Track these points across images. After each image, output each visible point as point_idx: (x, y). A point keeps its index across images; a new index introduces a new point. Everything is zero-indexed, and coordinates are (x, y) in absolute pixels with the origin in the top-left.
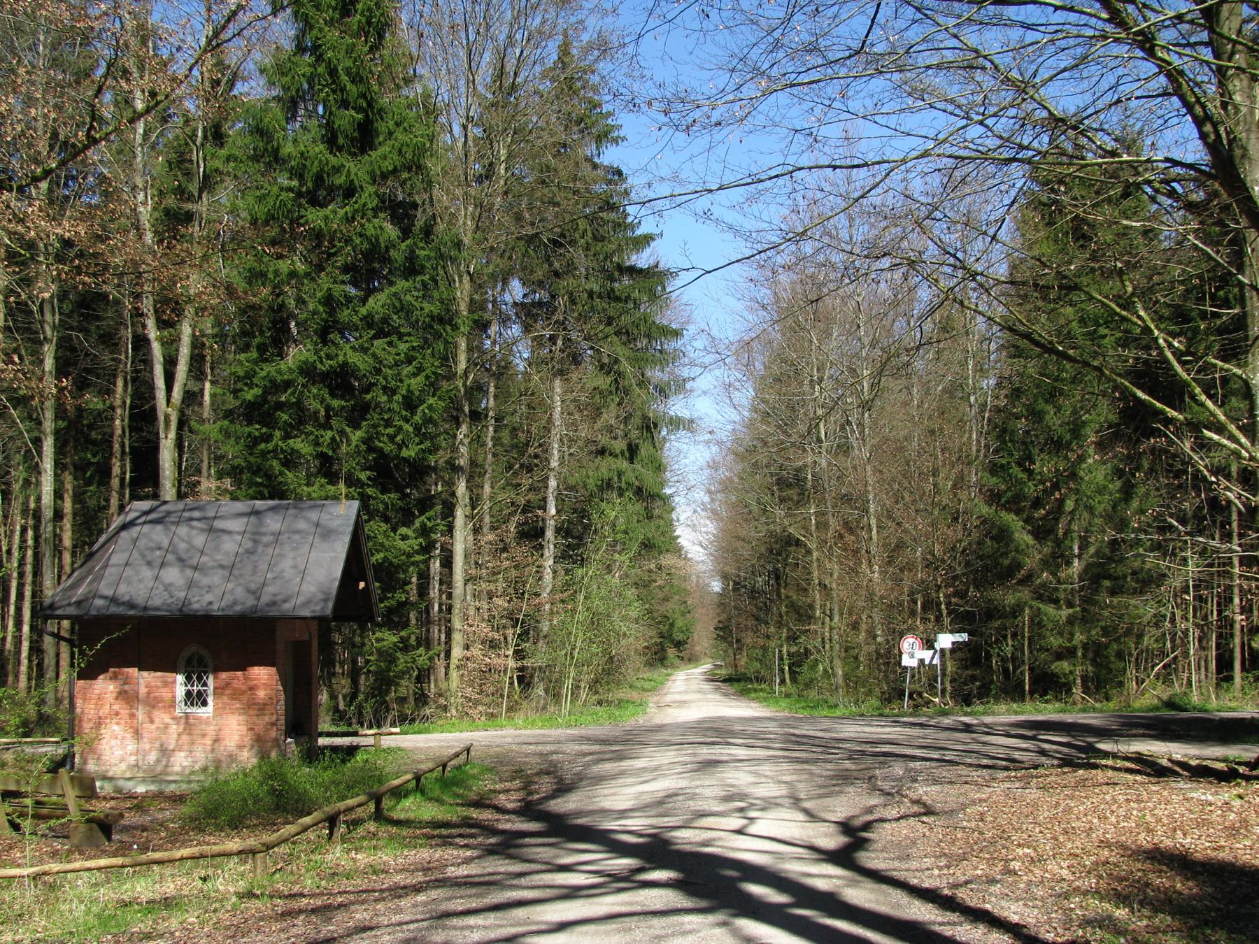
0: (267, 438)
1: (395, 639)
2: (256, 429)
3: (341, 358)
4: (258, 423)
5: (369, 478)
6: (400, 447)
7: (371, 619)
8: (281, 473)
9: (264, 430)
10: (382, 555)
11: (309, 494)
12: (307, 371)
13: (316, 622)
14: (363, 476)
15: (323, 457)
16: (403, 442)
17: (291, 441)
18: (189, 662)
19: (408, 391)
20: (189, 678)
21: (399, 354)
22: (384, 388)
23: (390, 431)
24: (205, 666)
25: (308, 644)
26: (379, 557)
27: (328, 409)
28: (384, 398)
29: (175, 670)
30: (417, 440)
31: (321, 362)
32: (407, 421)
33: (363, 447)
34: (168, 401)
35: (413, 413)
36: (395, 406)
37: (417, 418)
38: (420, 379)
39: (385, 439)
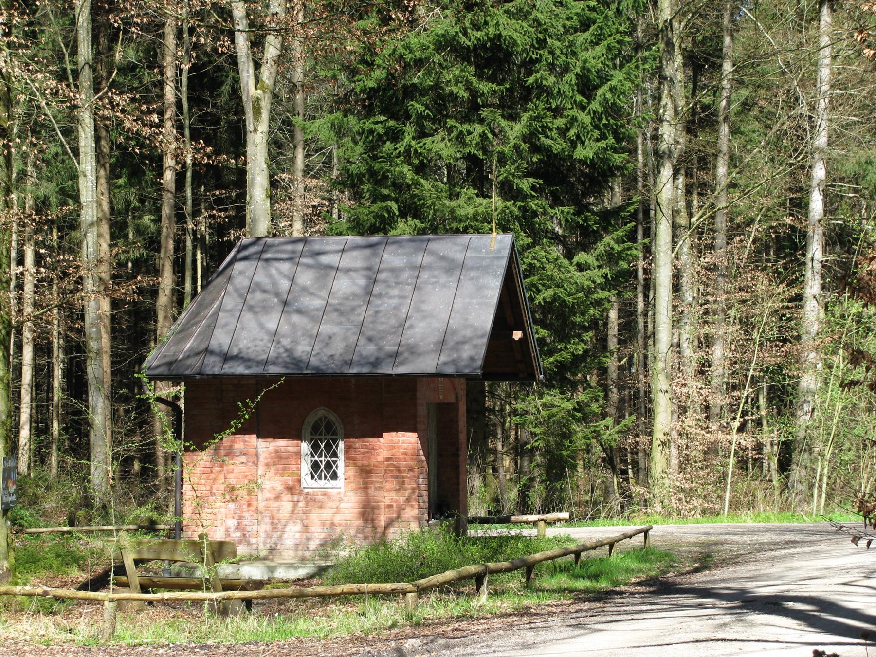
0: (395, 136)
1: (569, 406)
2: (379, 123)
3: (491, 30)
4: (382, 113)
5: (533, 188)
6: (573, 145)
7: (532, 376)
8: (417, 184)
9: (392, 123)
10: (551, 292)
11: (452, 211)
12: (445, 44)
13: (463, 380)
14: (525, 184)
15: (471, 158)
16: (578, 136)
17: (428, 140)
18: (315, 429)
19: (583, 68)
20: (315, 447)
21: (569, 19)
22: (551, 67)
23: (560, 122)
24: (335, 433)
25: (453, 407)
26: (547, 294)
27: (474, 94)
28: (552, 79)
29: (298, 436)
30: (596, 134)
31: (465, 34)
32: (583, 108)
33: (525, 146)
34: (257, 79)
35: (590, 97)
36: (566, 89)
37: (595, 106)
38: (600, 49)
39: (554, 134)
